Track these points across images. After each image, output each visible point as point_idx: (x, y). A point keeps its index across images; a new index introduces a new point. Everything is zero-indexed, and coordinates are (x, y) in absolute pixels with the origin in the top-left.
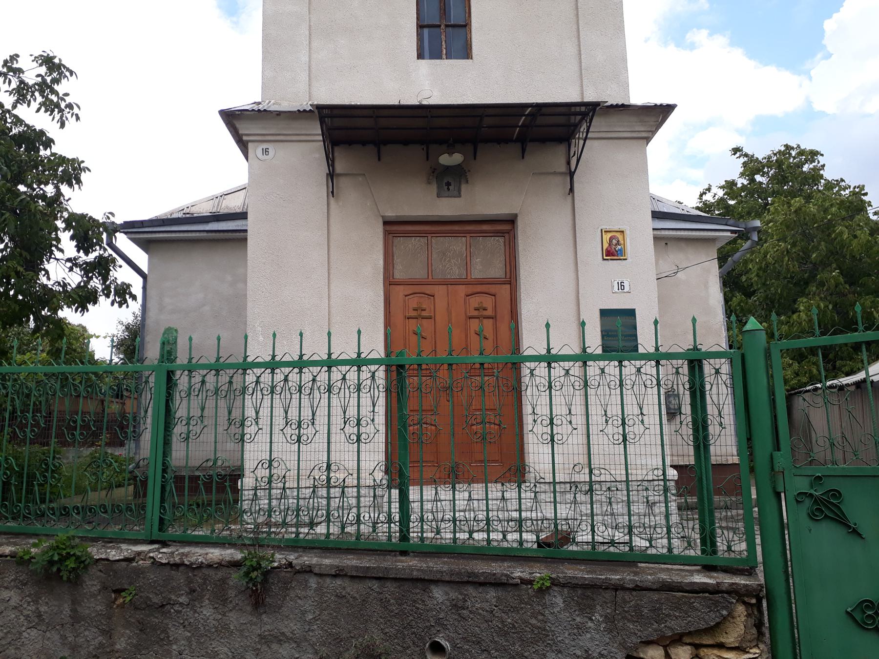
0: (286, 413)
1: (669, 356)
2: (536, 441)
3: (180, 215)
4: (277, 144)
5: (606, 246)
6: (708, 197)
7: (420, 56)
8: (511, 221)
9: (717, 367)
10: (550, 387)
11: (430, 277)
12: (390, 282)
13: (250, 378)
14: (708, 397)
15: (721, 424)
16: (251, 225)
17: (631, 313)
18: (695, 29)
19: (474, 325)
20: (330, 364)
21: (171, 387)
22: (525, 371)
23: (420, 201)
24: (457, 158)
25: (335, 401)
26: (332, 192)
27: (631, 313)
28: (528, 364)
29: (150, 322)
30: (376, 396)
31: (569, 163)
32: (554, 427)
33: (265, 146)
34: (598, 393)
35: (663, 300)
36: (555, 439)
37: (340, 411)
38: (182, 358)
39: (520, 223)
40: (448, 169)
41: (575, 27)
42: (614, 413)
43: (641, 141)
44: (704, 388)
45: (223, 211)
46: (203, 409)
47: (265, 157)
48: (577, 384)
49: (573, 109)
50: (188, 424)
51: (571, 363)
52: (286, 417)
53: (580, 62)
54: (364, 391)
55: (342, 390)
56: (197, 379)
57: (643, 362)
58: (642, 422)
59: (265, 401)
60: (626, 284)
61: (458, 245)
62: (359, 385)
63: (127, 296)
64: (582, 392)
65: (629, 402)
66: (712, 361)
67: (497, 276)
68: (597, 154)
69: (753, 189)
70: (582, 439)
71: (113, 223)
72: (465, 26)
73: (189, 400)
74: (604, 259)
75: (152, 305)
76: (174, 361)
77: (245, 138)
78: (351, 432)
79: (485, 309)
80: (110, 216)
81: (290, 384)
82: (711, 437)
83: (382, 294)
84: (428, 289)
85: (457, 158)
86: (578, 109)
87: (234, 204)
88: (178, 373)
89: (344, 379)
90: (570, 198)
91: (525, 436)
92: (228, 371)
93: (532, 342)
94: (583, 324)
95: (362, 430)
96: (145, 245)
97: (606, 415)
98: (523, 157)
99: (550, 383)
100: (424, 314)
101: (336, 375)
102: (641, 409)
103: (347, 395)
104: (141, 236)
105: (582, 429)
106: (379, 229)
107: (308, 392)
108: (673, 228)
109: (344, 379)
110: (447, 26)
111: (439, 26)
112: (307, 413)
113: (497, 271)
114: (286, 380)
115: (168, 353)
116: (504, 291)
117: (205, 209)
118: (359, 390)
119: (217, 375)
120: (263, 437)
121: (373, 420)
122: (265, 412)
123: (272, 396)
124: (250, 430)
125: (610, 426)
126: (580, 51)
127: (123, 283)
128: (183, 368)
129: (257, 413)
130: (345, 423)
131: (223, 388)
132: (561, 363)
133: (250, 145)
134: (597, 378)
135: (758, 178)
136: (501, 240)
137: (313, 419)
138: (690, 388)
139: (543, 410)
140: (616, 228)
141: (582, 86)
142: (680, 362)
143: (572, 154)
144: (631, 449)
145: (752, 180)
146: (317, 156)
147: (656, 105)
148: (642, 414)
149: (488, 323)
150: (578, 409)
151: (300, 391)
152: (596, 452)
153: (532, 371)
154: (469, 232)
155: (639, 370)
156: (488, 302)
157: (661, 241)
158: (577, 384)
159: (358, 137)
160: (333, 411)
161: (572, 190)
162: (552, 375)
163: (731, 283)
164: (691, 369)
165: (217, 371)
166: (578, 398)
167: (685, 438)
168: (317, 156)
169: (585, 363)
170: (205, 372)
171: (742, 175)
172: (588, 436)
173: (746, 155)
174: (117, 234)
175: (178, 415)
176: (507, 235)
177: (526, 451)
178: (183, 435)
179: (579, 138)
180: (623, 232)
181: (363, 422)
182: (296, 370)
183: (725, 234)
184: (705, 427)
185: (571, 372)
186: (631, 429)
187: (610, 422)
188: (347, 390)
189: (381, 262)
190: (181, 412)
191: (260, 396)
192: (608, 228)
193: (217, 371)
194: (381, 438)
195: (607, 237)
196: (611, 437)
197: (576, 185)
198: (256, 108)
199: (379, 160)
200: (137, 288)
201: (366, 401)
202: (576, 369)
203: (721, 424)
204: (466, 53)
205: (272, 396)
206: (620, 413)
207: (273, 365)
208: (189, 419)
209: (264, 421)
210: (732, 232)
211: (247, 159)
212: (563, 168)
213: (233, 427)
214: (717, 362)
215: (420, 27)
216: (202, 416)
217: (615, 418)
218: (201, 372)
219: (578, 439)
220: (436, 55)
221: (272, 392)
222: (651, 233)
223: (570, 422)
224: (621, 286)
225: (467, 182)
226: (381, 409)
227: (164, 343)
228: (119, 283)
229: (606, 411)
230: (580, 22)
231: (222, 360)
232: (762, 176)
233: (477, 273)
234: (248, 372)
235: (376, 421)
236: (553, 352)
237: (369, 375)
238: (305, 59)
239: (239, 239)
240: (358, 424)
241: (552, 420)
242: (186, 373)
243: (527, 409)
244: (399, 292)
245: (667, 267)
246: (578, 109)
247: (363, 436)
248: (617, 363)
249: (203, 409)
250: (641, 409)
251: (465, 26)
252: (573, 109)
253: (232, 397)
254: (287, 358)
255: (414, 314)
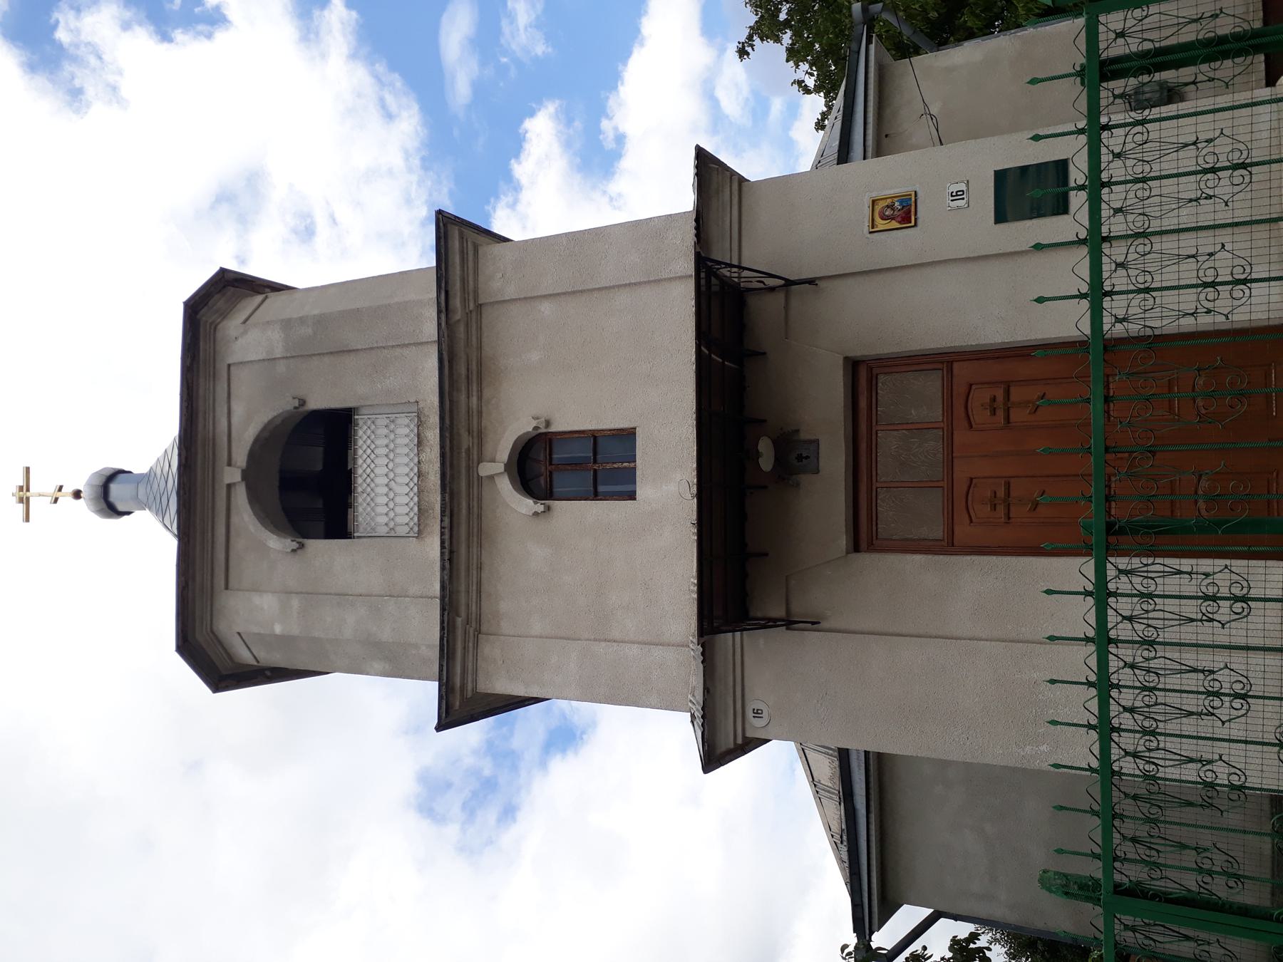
0: (1191, 714)
1: (1094, 111)
2: (1246, 309)
3: (844, 849)
4: (747, 697)
5: (895, 224)
6: (811, 82)
7: (632, 496)
8: (854, 366)
9: (1113, 36)
10: (1147, 290)
11: (940, 484)
12: (949, 545)
13: (1128, 766)
14: (1163, 44)
15: (1215, 16)
16: (858, 745)
17: (1000, 176)
18: (601, 137)
19: (1018, 416)
20: (1103, 640)
21: (1142, 891)
22: (1119, 330)
23: (824, 499)
24: (765, 448)
25: (1170, 635)
26: (813, 623)
27: (1000, 176)
28: (1106, 327)
29: (1012, 918)
30: (1161, 568)
31: (772, 289)
32: (1218, 280)
33: (750, 714)
34: (1158, 214)
35: (975, 131)
36: (1243, 277)
37: (1190, 628)
38: (1094, 870)
39: (857, 352)
40: (780, 460)
41: (596, 294)
42: (1194, 186)
43: (744, 189)
44: (1149, 51)
45: (837, 785)
46: (1183, 846)
47: (765, 714)
48: (1140, 249)
49: (703, 289)
50: (1210, 873)
51: (1105, 259)
52: (1200, 714)
53: (640, 283)
54: (1153, 588)
55: (1150, 622)
56: (1128, 849)
57: (1104, 150)
58: (1209, 141)
59: (1169, 746)
60: (954, 188)
61: (889, 443)
62: (1142, 595)
63: (972, 946)
64: (1154, 239)
65: (1174, 164)
66: (1102, 46)
67: (939, 383)
68: (762, 249)
69: (799, 23)
70: (1242, 234)
71: (856, 947)
72: (595, 438)
73: (1165, 865)
74: (916, 225)
75: (983, 911)
76: (1097, 883)
77: (740, 741)
78: (1227, 610)
79: (994, 399)
80: (846, 951)
81: (1138, 704)
82: (1238, 29)
83: (968, 558)
84: (960, 489)
85: (765, 448)
86: (703, 282)
87: (827, 768)
88: (1117, 877)
89: (1130, 619)
90: (822, 284)
91: (1236, 326)
92: (1115, 800)
93: (1070, 322)
94: (1038, 247)
95: (1224, 592)
96: (888, 910)
97: (1197, 200)
98: (764, 353)
99: (1139, 291)
100: (1001, 493)
101: (1123, 631)
102: (1186, 145)
103: (1160, 615)
104: (875, 909)
105: (1225, 236)
106: (865, 559)
107: (1153, 677)
108: (860, 131)
109: (1130, 619)
110: (595, 462)
111: (595, 471)
112: (1192, 681)
113: (930, 385)
114: (1131, 710)
115: (1084, 890)
116: (962, 371)
117: (836, 811)
118: (1151, 596)
119: (1122, 817)
120: (1236, 754)
121: (1207, 575)
122: (1189, 748)
123: (1161, 734)
124: (1222, 775)
125: (1218, 191)
126: (625, 285)
127: (951, 948)
128: (1109, 870)
129: (1191, 760)
130: (1211, 620)
131: (1145, 811)
132: (1105, 275)
133: (749, 734)
134: (1130, 218)
135: (783, 16)
136: (882, 378)
137: (1203, 671)
138: (1149, 73)
139: (1188, 300)
140: (867, 211)
141: (670, 279)
142: (1103, 94)
143: (761, 285)
144: (1257, 156)
145: (787, 24)
146: (761, 641)
147: (697, 174)
148: (1195, 143)
149: (1017, 394)
150: (1188, 243)
151: (1152, 689)
152: (1247, 212)
153: (1119, 320)
154: (870, 500)
155: (1118, 156)
156: (980, 397)
157: (881, 146)
158: (1140, 249)
159: (740, 585)
160: (1191, 638)
161: (811, 282)
162: (1124, 288)
163: (944, 32)
164: (1116, 75)
165: (1114, 816)
166: (1165, 246)
167: (1237, 70)
168: (761, 641)
169: (1105, 239)
170: (1116, 835)
171: (778, 40)
172: (1237, 224)
173: (750, 38)
174: (874, 945)
175: (1195, 888)
176: (874, 372)
177: (1247, 325)
178: (1231, 883)
179: (739, 277)
180: (874, 202)
181: (1211, 591)
182: (1114, 693)
183: (870, 54)
184: (1222, 40)
185: (1120, 259)
186: (1222, 158)
187: (1210, 192)
188: (1151, 615)
189: (918, 558)
190: (1191, 882)
191: (1160, 754)
192: (867, 223)
193: (1114, 816)
194: (1238, 565)
195: (881, 224)
196: (1237, 189)
197: (804, 276)
198: (699, 721)
199: (766, 555)
200: (963, 930)
201: (1172, 585)
202: (1114, 252)
203: (1215, 16)
204: (627, 437)
205: (1161, 734)
206: (1192, 178)
207: (1105, 729)
208: (1200, 870)
209: (1206, 750)
210: (869, 42)
211: (768, 741)
212: (780, 297)
213: (1215, 802)
214: (1104, 37)
215: (596, 496)
216: (1196, 849)
217: (1202, 186)
218: (1116, 841)
219: (1238, 241)
220: (630, 476)
221: (1153, 733)
222: (872, 162)
223: (1211, 255)
224: (957, 195)
225: (798, 431)
226: (1186, 564)
227: (1066, 894)
228: (950, 955)
229: (1191, 200)
230: (590, 287)
231: (1096, 808)
232: (780, 11)
233: (936, 413)
234: (1116, 769)
235: (1209, 570)
236: (1085, 289)
237: (1124, 578)
238: (634, 650)
239: (879, 764)
240: (1214, 598)
241: (1206, 285)
242: (1117, 864)
243: (1188, 324)
244: (963, 531)
245: (923, 130)
246: (703, 282)
247: (1236, 591)
248: (1105, 190)
249: (1183, 846)
250: (1186, 145)
251: (595, 438)
252: (703, 289)
253: (1161, 797)
254: (1094, 706)
255: (1001, 509)
